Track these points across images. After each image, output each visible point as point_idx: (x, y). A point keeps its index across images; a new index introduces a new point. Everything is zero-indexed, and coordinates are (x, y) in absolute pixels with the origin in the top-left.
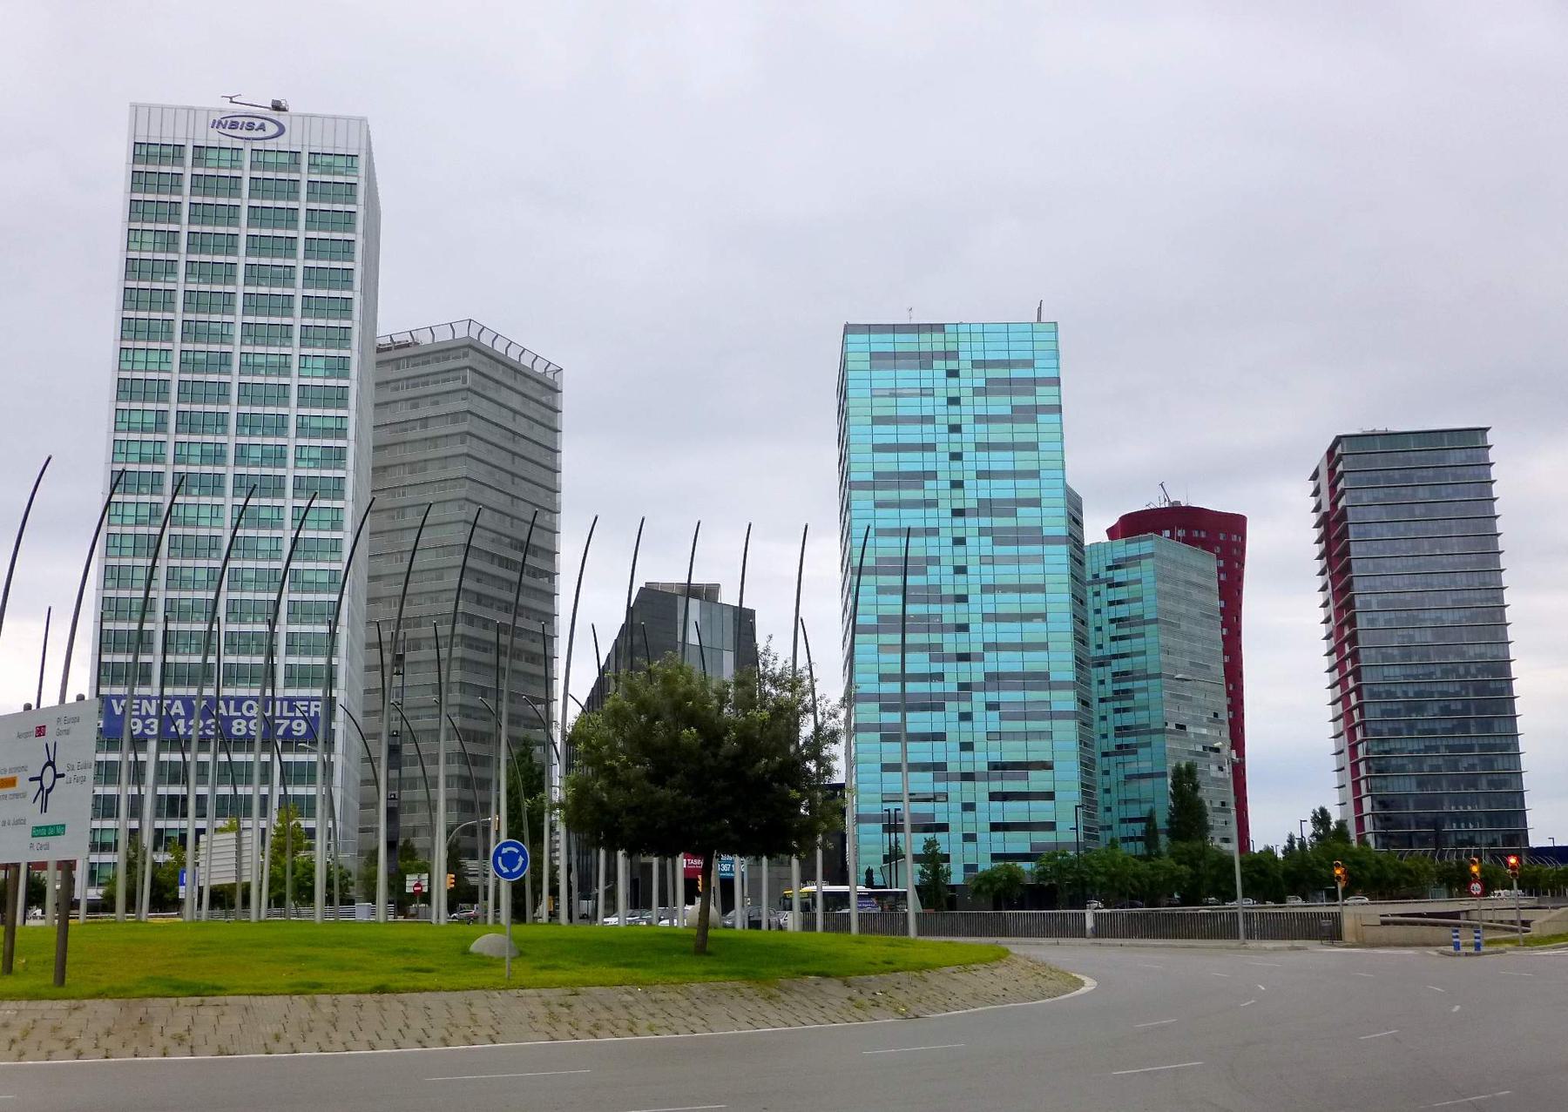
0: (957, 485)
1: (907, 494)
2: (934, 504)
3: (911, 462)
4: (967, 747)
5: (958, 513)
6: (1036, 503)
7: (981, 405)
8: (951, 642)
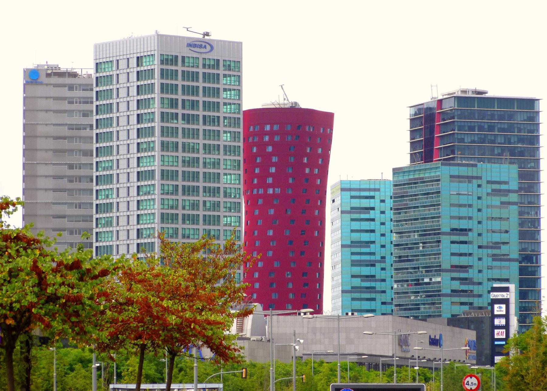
1: (363, 216)
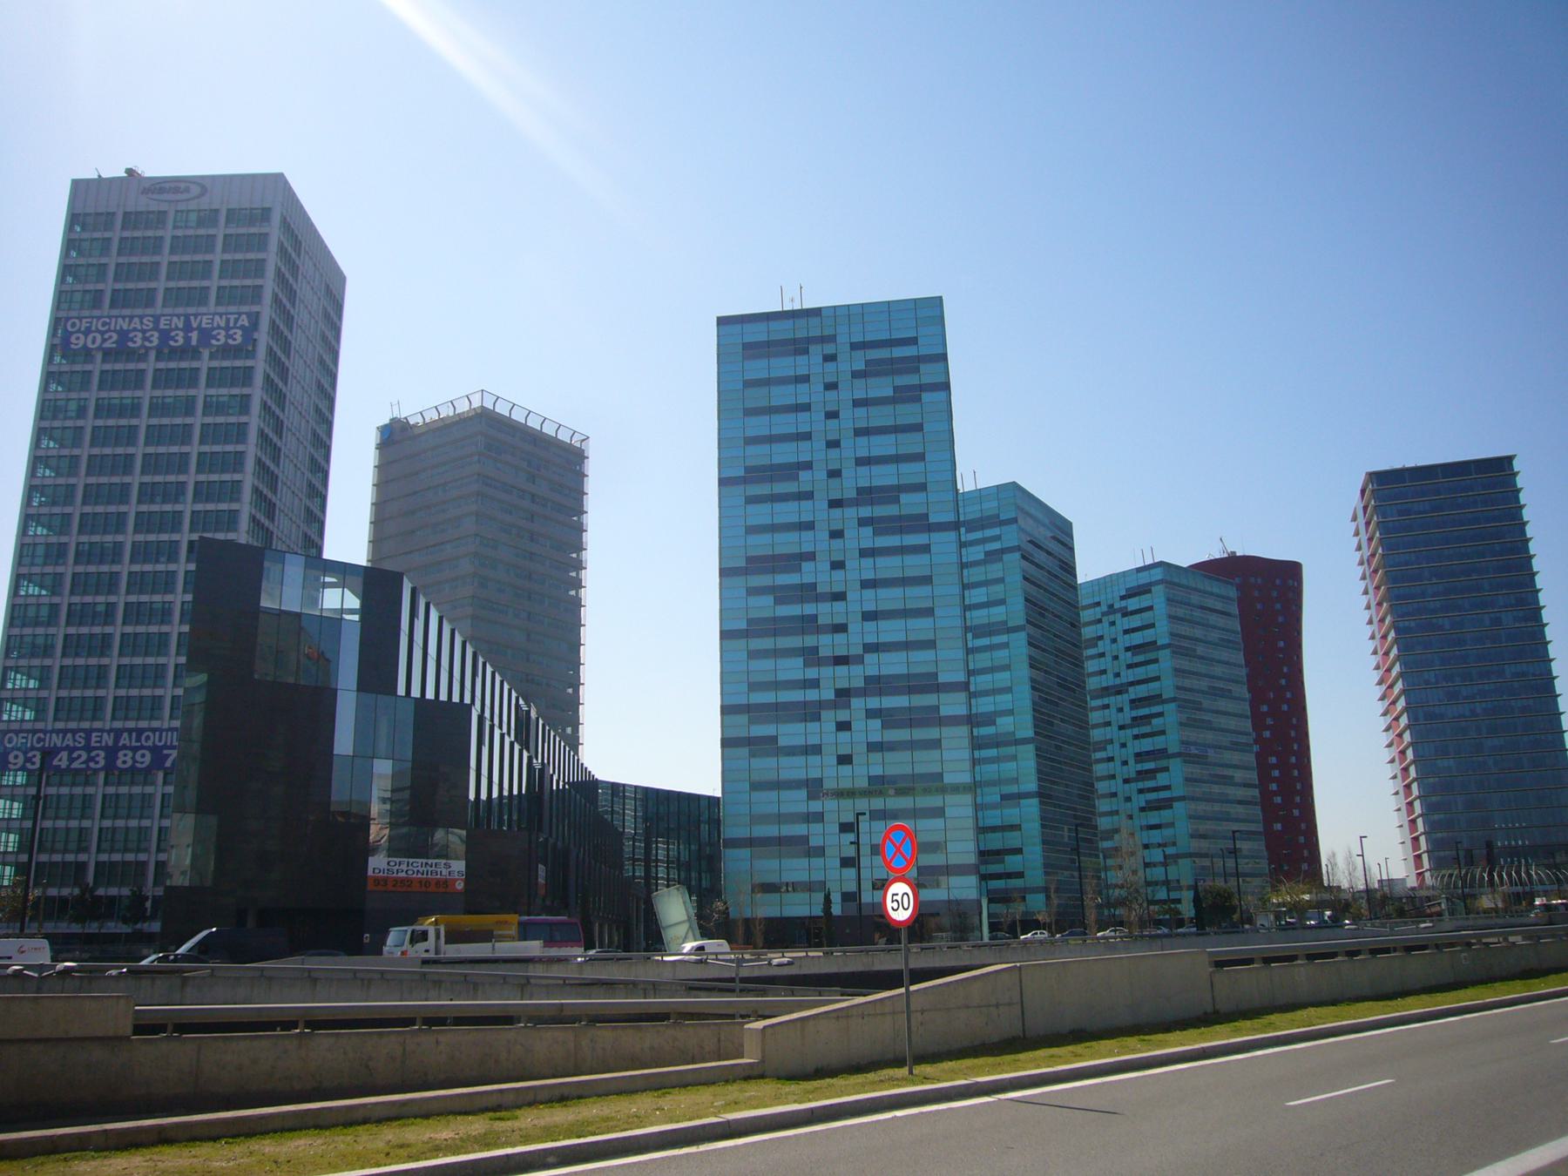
0: (834, 474)
2: (809, 496)
3: (785, 454)
4: (845, 760)
5: (835, 504)
6: (922, 487)
7: (860, 390)
8: (828, 644)
